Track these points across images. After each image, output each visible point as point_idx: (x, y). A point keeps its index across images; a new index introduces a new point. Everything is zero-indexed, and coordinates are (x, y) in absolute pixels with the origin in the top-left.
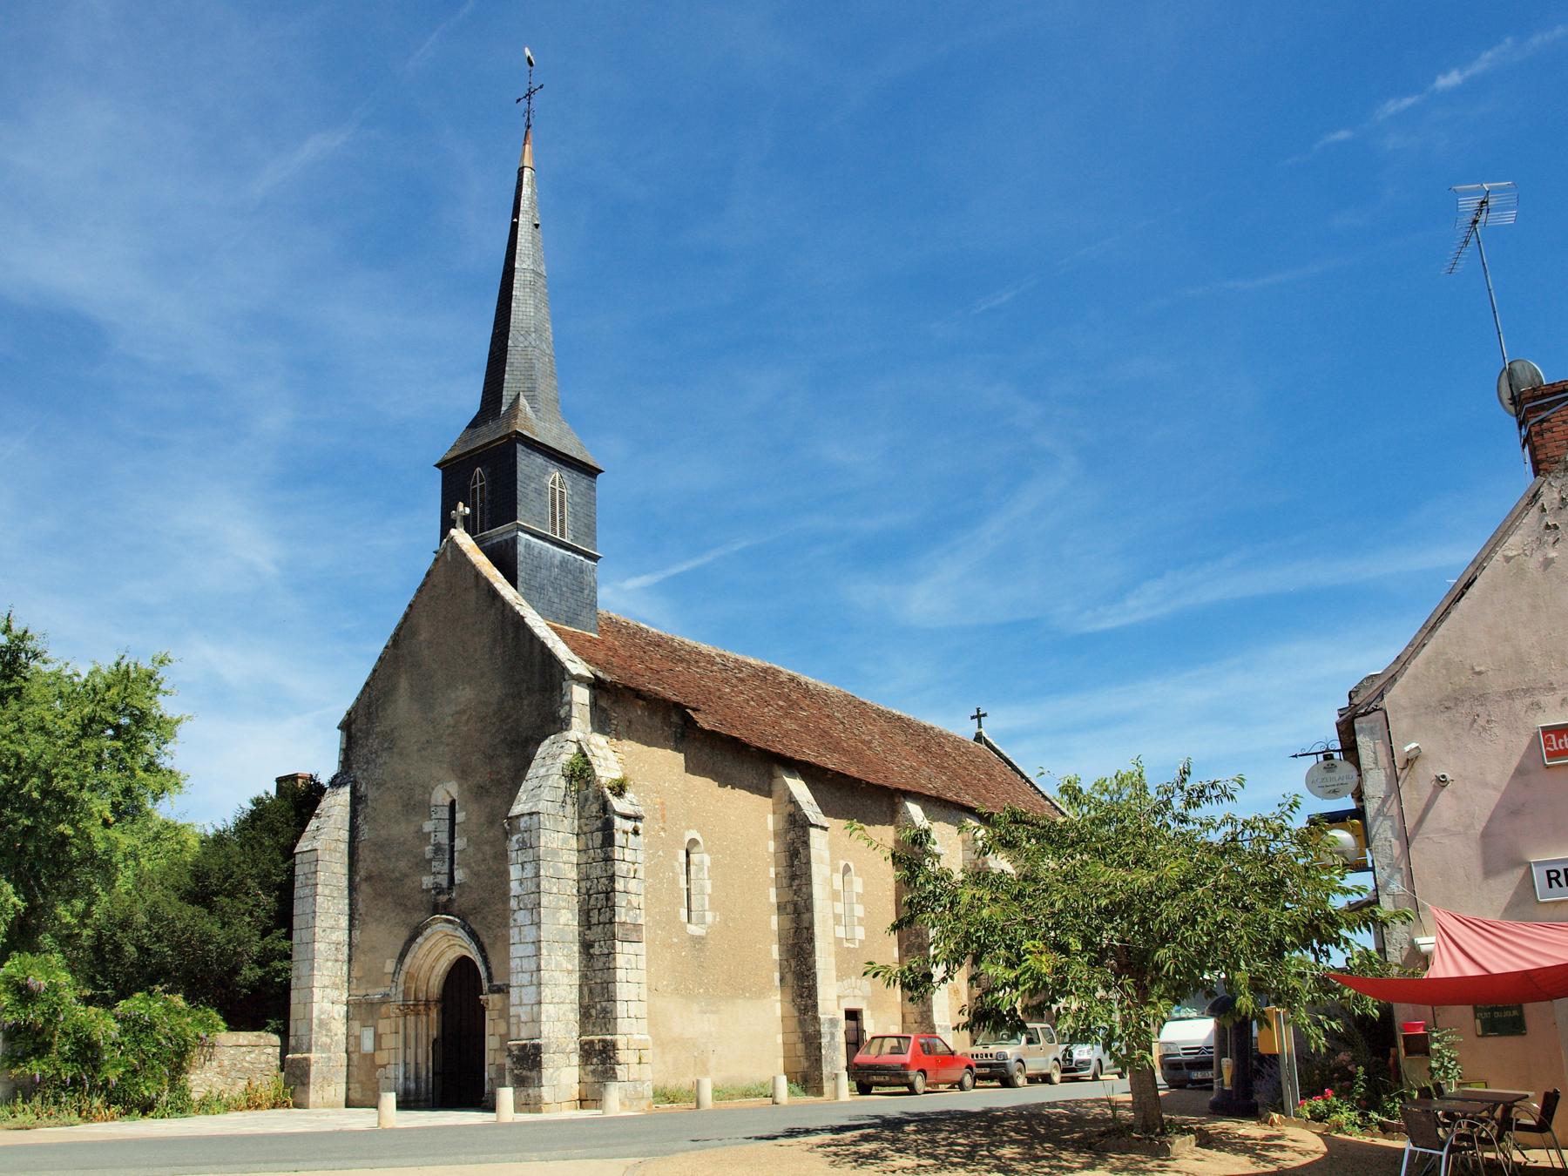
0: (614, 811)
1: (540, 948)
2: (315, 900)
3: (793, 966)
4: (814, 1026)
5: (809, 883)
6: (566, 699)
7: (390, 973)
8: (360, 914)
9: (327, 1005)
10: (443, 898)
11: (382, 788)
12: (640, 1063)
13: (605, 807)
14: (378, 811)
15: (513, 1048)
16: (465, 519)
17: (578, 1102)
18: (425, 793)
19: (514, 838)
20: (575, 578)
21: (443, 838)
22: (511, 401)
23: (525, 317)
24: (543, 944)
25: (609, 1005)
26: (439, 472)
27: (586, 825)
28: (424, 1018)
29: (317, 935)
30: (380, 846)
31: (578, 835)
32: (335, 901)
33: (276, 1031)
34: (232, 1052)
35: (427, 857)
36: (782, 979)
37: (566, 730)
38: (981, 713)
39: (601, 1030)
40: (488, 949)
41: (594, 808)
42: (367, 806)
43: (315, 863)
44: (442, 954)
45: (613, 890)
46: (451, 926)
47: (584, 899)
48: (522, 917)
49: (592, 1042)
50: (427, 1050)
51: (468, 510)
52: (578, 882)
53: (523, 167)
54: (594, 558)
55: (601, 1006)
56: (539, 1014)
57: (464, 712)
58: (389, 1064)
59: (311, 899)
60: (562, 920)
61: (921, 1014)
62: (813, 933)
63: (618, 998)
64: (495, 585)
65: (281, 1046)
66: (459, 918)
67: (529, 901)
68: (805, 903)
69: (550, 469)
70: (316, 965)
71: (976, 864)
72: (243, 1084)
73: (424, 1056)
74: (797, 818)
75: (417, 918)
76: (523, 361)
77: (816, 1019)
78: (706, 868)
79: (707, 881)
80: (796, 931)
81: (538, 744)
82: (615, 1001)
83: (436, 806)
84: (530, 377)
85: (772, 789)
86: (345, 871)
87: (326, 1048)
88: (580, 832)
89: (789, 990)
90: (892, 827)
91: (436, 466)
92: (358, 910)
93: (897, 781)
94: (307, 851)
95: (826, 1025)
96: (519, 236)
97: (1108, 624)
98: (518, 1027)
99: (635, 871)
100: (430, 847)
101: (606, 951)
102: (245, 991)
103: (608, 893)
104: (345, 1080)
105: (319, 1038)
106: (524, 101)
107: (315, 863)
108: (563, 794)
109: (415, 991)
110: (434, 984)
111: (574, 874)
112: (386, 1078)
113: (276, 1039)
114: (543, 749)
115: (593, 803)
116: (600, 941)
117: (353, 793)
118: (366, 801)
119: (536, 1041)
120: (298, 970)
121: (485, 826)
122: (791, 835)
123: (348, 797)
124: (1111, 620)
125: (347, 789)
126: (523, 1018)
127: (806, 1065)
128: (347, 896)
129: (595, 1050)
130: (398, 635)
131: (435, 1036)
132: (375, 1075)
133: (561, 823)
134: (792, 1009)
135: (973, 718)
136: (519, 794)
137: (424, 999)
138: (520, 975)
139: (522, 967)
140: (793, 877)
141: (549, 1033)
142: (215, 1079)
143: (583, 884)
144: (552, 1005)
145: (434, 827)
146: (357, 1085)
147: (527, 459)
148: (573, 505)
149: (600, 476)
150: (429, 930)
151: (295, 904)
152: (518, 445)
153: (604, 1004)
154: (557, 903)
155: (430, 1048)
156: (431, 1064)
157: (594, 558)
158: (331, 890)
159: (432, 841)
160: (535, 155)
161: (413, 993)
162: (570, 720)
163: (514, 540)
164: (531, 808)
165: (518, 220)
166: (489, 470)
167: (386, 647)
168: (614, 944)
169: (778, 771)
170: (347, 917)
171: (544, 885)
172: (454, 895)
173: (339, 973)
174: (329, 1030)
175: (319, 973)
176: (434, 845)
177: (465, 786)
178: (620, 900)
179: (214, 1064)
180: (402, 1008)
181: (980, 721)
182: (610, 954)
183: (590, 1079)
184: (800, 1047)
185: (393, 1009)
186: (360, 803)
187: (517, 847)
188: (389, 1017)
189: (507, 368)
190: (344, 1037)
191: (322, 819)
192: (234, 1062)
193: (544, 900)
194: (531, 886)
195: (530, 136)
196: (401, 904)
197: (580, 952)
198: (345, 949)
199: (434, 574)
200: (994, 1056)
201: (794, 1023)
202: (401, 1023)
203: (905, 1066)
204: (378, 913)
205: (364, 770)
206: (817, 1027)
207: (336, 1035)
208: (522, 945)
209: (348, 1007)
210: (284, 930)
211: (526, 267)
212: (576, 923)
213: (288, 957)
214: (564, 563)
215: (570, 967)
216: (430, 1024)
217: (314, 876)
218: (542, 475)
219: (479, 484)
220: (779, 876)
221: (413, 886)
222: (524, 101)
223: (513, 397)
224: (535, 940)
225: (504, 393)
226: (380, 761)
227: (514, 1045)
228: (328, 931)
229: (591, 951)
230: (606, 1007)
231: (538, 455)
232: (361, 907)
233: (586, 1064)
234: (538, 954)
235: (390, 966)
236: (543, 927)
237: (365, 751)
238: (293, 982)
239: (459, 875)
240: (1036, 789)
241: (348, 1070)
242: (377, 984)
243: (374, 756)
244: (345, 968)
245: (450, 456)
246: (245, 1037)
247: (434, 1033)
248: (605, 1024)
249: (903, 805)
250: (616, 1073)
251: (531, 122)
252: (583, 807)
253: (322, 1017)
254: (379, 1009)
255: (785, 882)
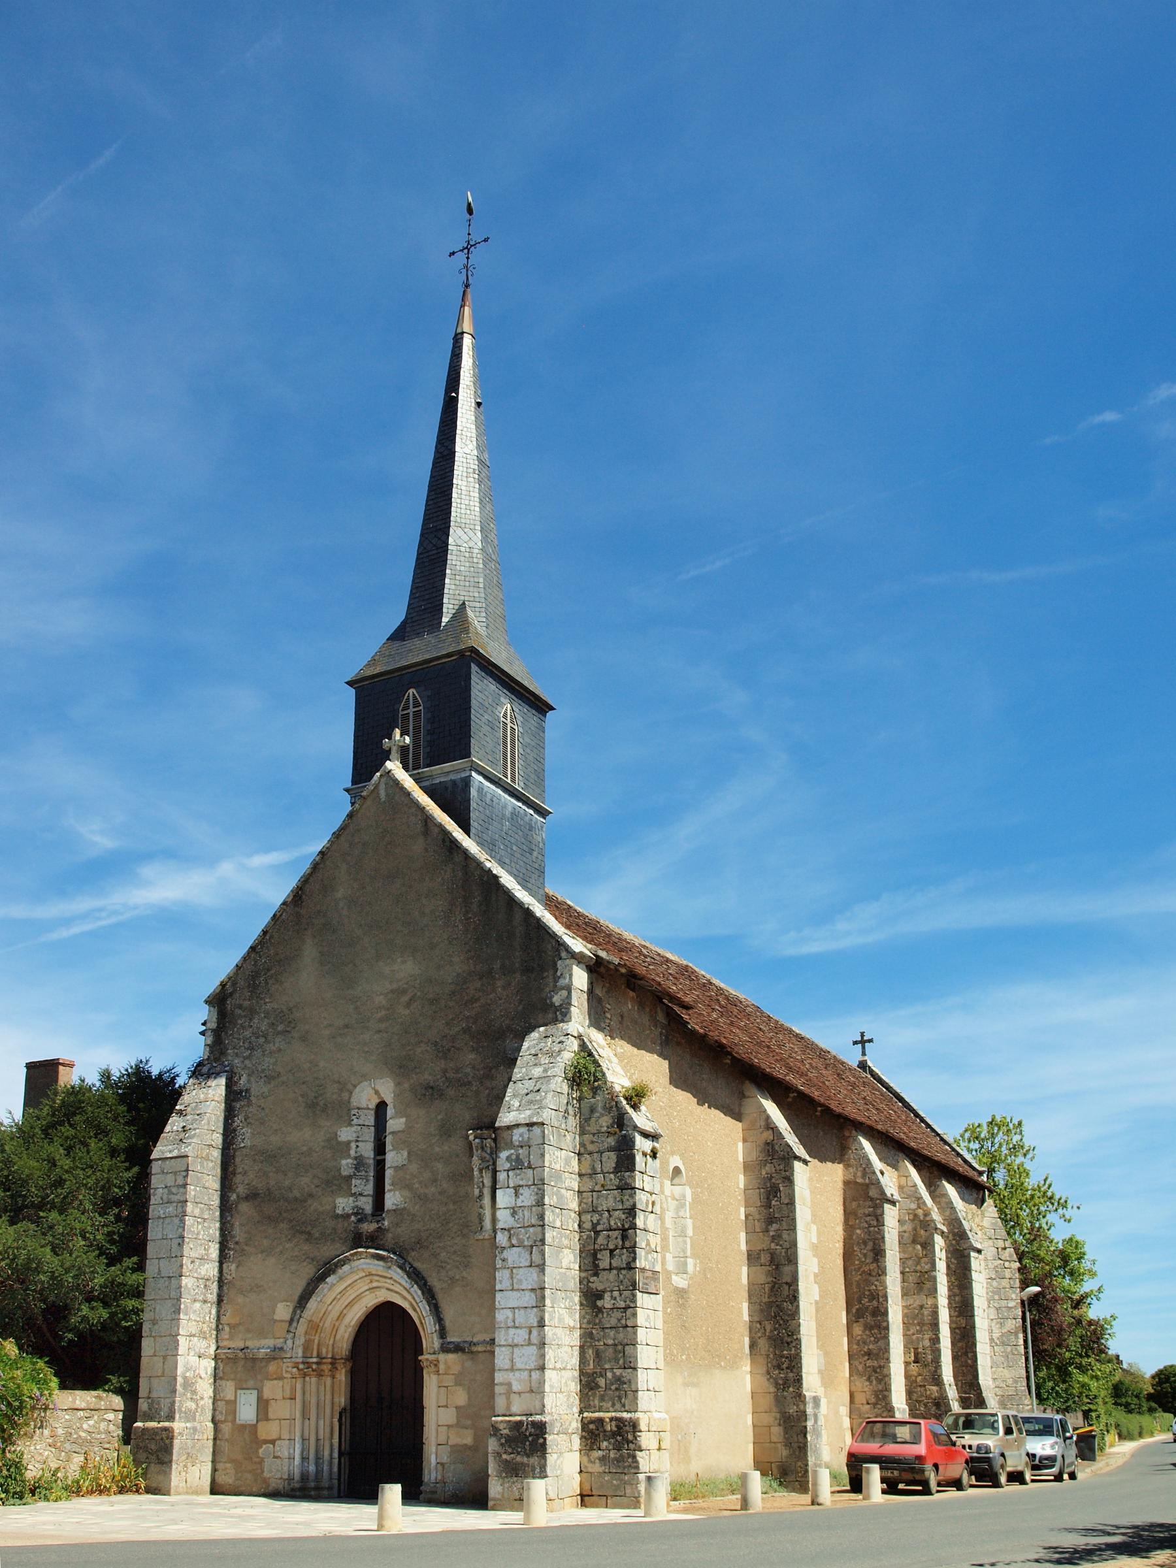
0: (635, 1127)
1: (543, 1297)
2: (183, 1221)
3: (768, 1331)
4: (797, 1406)
5: (792, 1228)
6: (562, 982)
7: (286, 1321)
8: (237, 1243)
9: (193, 1360)
10: (369, 1227)
11: (273, 1082)
12: (659, 1449)
13: (621, 1120)
14: (267, 1111)
15: (501, 1426)
16: (404, 750)
17: (579, 1497)
18: (341, 1090)
19: (504, 1155)
20: (526, 836)
21: (367, 1150)
22: (454, 611)
23: (468, 512)
24: (547, 1292)
25: (627, 1374)
26: (352, 692)
27: (592, 1142)
28: (329, 1381)
29: (184, 1267)
30: (268, 1156)
31: (579, 1154)
32: (206, 1224)
33: (119, 1391)
34: (67, 1417)
35: (345, 1173)
36: (753, 1345)
37: (563, 1021)
38: (865, 1038)
39: (613, 1405)
40: (440, 1296)
41: (605, 1122)
42: (249, 1104)
43: (184, 1174)
44: (358, 1297)
45: (634, 1227)
46: (381, 1263)
47: (589, 1237)
48: (514, 1256)
49: (601, 1421)
50: (332, 1423)
51: (407, 740)
52: (579, 1215)
53: (463, 333)
54: (543, 813)
55: (614, 1373)
56: (542, 1382)
57: (404, 991)
58: (280, 1439)
59: (176, 1221)
60: (565, 1263)
61: (876, 1394)
62: (796, 1291)
63: (639, 1366)
64: (454, 834)
65: (124, 1411)
66: (394, 1253)
67: (527, 1236)
68: (786, 1252)
69: (502, 699)
70: (182, 1306)
71: (916, 1215)
72: (78, 1459)
73: (328, 1430)
74: (777, 1148)
75: (327, 1251)
76: (467, 564)
77: (800, 1396)
78: (687, 1203)
79: (688, 1220)
80: (773, 1287)
81: (522, 1036)
82: (635, 1369)
83: (359, 1108)
84: (477, 585)
85: (742, 1111)
86: (217, 1186)
87: (190, 1416)
88: (582, 1150)
89: (762, 1360)
90: (841, 1166)
91: (347, 683)
92: (234, 1237)
93: (851, 1111)
94: (171, 1158)
95: (811, 1405)
96: (459, 414)
97: (814, 948)
98: (508, 1398)
99: (653, 1203)
100: (350, 1161)
101: (622, 1305)
102: (70, 1336)
103: (624, 1230)
104: (210, 1458)
105: (184, 1403)
106: (461, 257)
107: (184, 1174)
108: (566, 1101)
109: (319, 1345)
110: (343, 1337)
111: (574, 1205)
112: (275, 1457)
113: (117, 1401)
114: (531, 1042)
115: (602, 1115)
116: (612, 1291)
117: (229, 1086)
118: (248, 1098)
119: (538, 1418)
120: (152, 1311)
121: (437, 1137)
122: (769, 1168)
123: (222, 1091)
124: (817, 943)
125: (222, 1081)
126: (516, 1387)
127: (785, 1453)
128: (218, 1219)
129: (605, 1431)
130: (301, 889)
131: (343, 1404)
132: (257, 1452)
133: (563, 1139)
134: (766, 1384)
135: (855, 1043)
136: (507, 1099)
137: (330, 1356)
138: (512, 1331)
139: (514, 1322)
140: (770, 1220)
141: (552, 1408)
142: (46, 1453)
143: (587, 1217)
144: (554, 1371)
145: (355, 1135)
146: (228, 1465)
147: (480, 683)
148: (525, 746)
149: (550, 714)
150: (346, 1268)
151: (150, 1225)
152: (473, 665)
153: (618, 1372)
154: (560, 1241)
155: (336, 1421)
156: (336, 1441)
157: (543, 813)
158: (202, 1210)
159: (352, 1153)
160: (476, 321)
161: (315, 1347)
162: (569, 1009)
163: (467, 782)
164: (530, 1117)
165: (457, 394)
166: (429, 693)
167: (284, 903)
168: (634, 1296)
169: (750, 1089)
170: (217, 1246)
171: (549, 1217)
172: (386, 1223)
173: (207, 1318)
174: (194, 1392)
175: (185, 1317)
176: (356, 1158)
177: (406, 1085)
178: (641, 1240)
179: (46, 1432)
180: (301, 1366)
181: (863, 1048)
182: (630, 1308)
183: (597, 1468)
184: (777, 1432)
185: (287, 1368)
186: (239, 1100)
187: (508, 1165)
188: (281, 1378)
189: (448, 571)
190: (211, 1401)
191: (188, 1117)
192: (70, 1430)
193: (549, 1235)
194: (530, 1217)
195: (469, 296)
196: (302, 1232)
197: (581, 1304)
198: (214, 1287)
199: (359, 815)
200: (974, 1448)
201: (767, 1401)
202: (299, 1386)
203: (920, 1459)
204: (266, 1242)
205: (245, 1058)
206: (802, 1407)
207: (202, 1398)
208: (515, 1293)
209: (216, 1363)
210: (135, 1259)
211: (468, 452)
212: (577, 1268)
213: (138, 1293)
214: (515, 814)
215: (572, 1324)
216: (336, 1388)
217: (182, 1190)
218: (495, 705)
219: (411, 710)
220: (750, 1218)
221: (321, 1209)
222: (461, 257)
223: (457, 607)
224: (535, 1286)
225: (445, 600)
226: (270, 1047)
227: (502, 1421)
228: (197, 1262)
229: (599, 1303)
230: (621, 1375)
231: (491, 679)
232: (238, 1232)
233: (592, 1449)
234: (540, 1305)
235: (283, 1311)
236: (548, 1270)
237: (248, 1033)
238: (146, 1328)
239: (392, 1199)
240: (933, 1130)
241: (215, 1445)
242: (262, 1334)
243: (262, 1040)
244: (214, 1311)
245: (369, 673)
246: (82, 1398)
247: (342, 1400)
248: (620, 1398)
249: (855, 1140)
250: (637, 1462)
251: (470, 281)
252: (587, 1120)
253: (188, 1374)
254: (266, 1366)
255: (758, 1226)
